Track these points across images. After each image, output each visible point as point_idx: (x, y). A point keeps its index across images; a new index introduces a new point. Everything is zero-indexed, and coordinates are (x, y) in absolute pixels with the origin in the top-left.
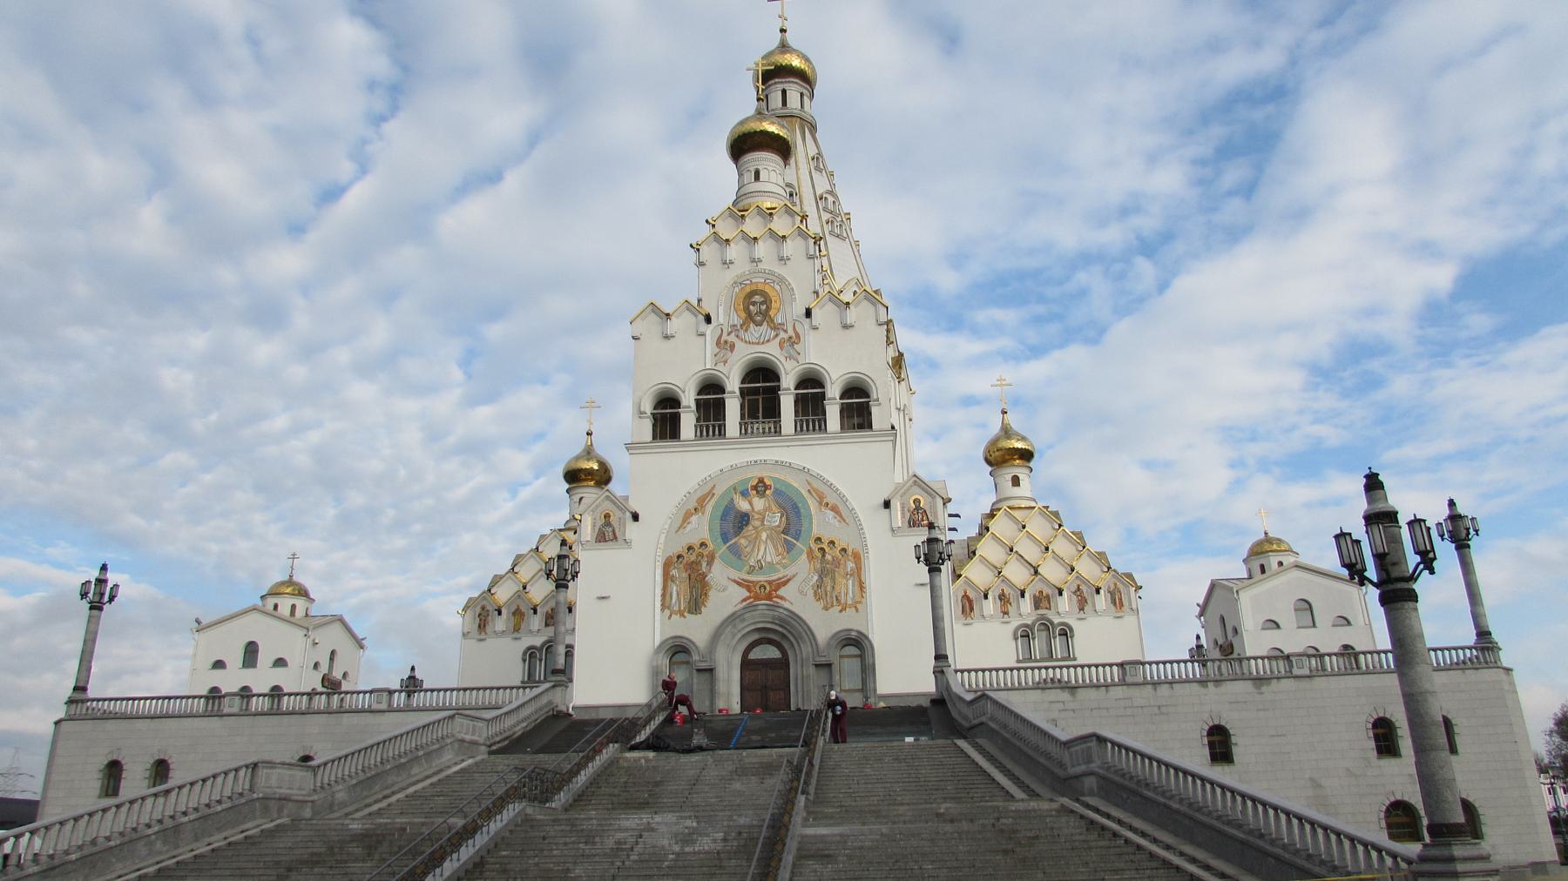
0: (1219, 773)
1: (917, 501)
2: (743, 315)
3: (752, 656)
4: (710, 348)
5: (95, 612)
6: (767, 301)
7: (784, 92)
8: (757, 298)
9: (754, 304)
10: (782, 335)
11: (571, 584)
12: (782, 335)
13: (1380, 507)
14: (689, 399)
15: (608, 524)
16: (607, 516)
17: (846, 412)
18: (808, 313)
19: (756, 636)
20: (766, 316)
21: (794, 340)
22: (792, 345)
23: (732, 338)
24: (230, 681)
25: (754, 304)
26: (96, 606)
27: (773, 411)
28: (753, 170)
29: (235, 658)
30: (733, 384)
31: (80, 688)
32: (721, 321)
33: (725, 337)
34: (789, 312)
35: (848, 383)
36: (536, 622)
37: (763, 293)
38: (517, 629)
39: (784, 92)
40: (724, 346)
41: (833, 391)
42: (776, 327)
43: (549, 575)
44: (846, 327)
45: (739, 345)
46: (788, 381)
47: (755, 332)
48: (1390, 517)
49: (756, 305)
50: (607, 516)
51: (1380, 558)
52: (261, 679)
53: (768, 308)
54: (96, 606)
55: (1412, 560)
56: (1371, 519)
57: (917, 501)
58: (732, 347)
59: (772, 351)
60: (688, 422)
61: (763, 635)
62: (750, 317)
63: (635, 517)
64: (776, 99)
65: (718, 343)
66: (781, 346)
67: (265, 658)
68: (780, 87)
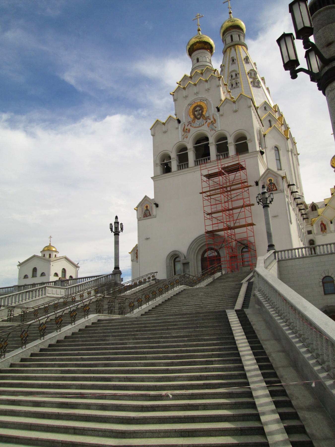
1: (270, 180)
2: (192, 117)
3: (206, 255)
5: (117, 236)
6: (202, 108)
7: (232, 37)
8: (198, 109)
11: (270, 205)
13: (94, 307)
14: (174, 155)
15: (147, 210)
16: (147, 207)
17: (207, 147)
18: (218, 110)
19: (206, 248)
20: (201, 115)
25: (196, 111)
26: (117, 234)
27: (207, 154)
28: (196, 58)
29: (30, 274)
30: (190, 146)
32: (184, 121)
34: (210, 111)
35: (236, 137)
39: (232, 37)
40: (186, 131)
41: (231, 140)
42: (207, 118)
46: (212, 140)
47: (197, 122)
48: (118, 223)
49: (198, 112)
50: (147, 207)
53: (202, 112)
54: (117, 234)
56: (115, 223)
57: (270, 180)
58: (189, 131)
59: (205, 130)
60: (174, 165)
61: (209, 247)
62: (195, 117)
63: (157, 205)
64: (228, 39)
65: (184, 130)
67: (39, 273)
68: (230, 34)
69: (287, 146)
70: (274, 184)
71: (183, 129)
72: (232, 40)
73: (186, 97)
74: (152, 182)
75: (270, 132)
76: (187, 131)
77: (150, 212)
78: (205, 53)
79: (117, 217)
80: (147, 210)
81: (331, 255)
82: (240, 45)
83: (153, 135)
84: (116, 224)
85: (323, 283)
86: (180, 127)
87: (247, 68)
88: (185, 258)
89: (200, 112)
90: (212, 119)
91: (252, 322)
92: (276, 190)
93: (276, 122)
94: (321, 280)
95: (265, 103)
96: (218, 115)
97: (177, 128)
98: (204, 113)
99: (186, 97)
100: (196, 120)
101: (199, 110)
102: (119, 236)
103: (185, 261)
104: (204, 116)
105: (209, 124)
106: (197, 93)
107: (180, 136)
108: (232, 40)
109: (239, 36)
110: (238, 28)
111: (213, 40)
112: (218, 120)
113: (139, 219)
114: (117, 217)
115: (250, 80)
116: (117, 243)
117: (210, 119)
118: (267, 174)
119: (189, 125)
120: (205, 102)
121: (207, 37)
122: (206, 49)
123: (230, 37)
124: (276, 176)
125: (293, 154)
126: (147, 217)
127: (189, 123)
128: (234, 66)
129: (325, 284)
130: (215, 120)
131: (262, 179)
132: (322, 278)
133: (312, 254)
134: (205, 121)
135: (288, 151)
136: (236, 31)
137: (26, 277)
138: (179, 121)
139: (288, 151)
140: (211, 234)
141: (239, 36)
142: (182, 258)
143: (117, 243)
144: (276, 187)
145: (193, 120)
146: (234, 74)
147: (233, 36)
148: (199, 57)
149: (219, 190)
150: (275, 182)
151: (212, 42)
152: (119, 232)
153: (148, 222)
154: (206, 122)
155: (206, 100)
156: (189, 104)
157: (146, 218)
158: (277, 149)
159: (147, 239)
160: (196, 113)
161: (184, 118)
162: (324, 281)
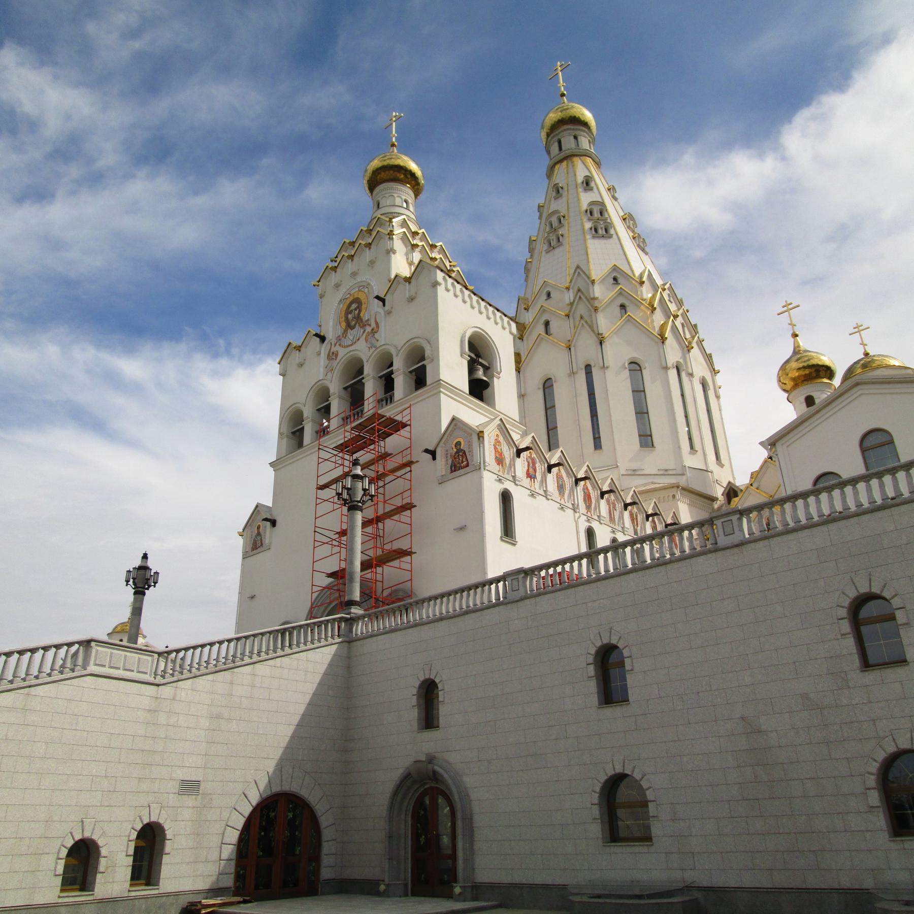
0: (574, 133)
2: (344, 324)
7: (560, 142)
8: (354, 306)
15: (259, 534)
20: (358, 318)
25: (351, 312)
47: (351, 334)
59: (362, 350)
64: (555, 148)
68: (556, 138)
69: (662, 356)
70: (464, 453)
72: (560, 149)
73: (337, 286)
74: (271, 472)
75: (617, 332)
78: (392, 188)
79: (145, 557)
80: (259, 534)
81: (440, 623)
82: (577, 156)
83: (283, 374)
87: (586, 199)
89: (357, 312)
90: (373, 325)
93: (639, 307)
95: (615, 268)
96: (382, 313)
98: (361, 315)
99: (337, 286)
100: (349, 331)
102: (146, 598)
104: (362, 320)
105: (369, 334)
106: (354, 275)
107: (322, 369)
108: (560, 149)
109: (576, 138)
110: (576, 122)
111: (417, 164)
113: (245, 556)
114: (145, 557)
115: (588, 225)
117: (370, 325)
118: (453, 431)
120: (366, 290)
121: (406, 158)
122: (402, 182)
123: (556, 144)
125: (683, 374)
127: (339, 339)
130: (377, 324)
131: (442, 444)
135: (666, 368)
136: (565, 130)
138: (323, 339)
139: (666, 368)
141: (576, 138)
144: (467, 460)
145: (345, 333)
151: (413, 166)
153: (262, 557)
157: (255, 552)
158: (635, 367)
161: (331, 329)
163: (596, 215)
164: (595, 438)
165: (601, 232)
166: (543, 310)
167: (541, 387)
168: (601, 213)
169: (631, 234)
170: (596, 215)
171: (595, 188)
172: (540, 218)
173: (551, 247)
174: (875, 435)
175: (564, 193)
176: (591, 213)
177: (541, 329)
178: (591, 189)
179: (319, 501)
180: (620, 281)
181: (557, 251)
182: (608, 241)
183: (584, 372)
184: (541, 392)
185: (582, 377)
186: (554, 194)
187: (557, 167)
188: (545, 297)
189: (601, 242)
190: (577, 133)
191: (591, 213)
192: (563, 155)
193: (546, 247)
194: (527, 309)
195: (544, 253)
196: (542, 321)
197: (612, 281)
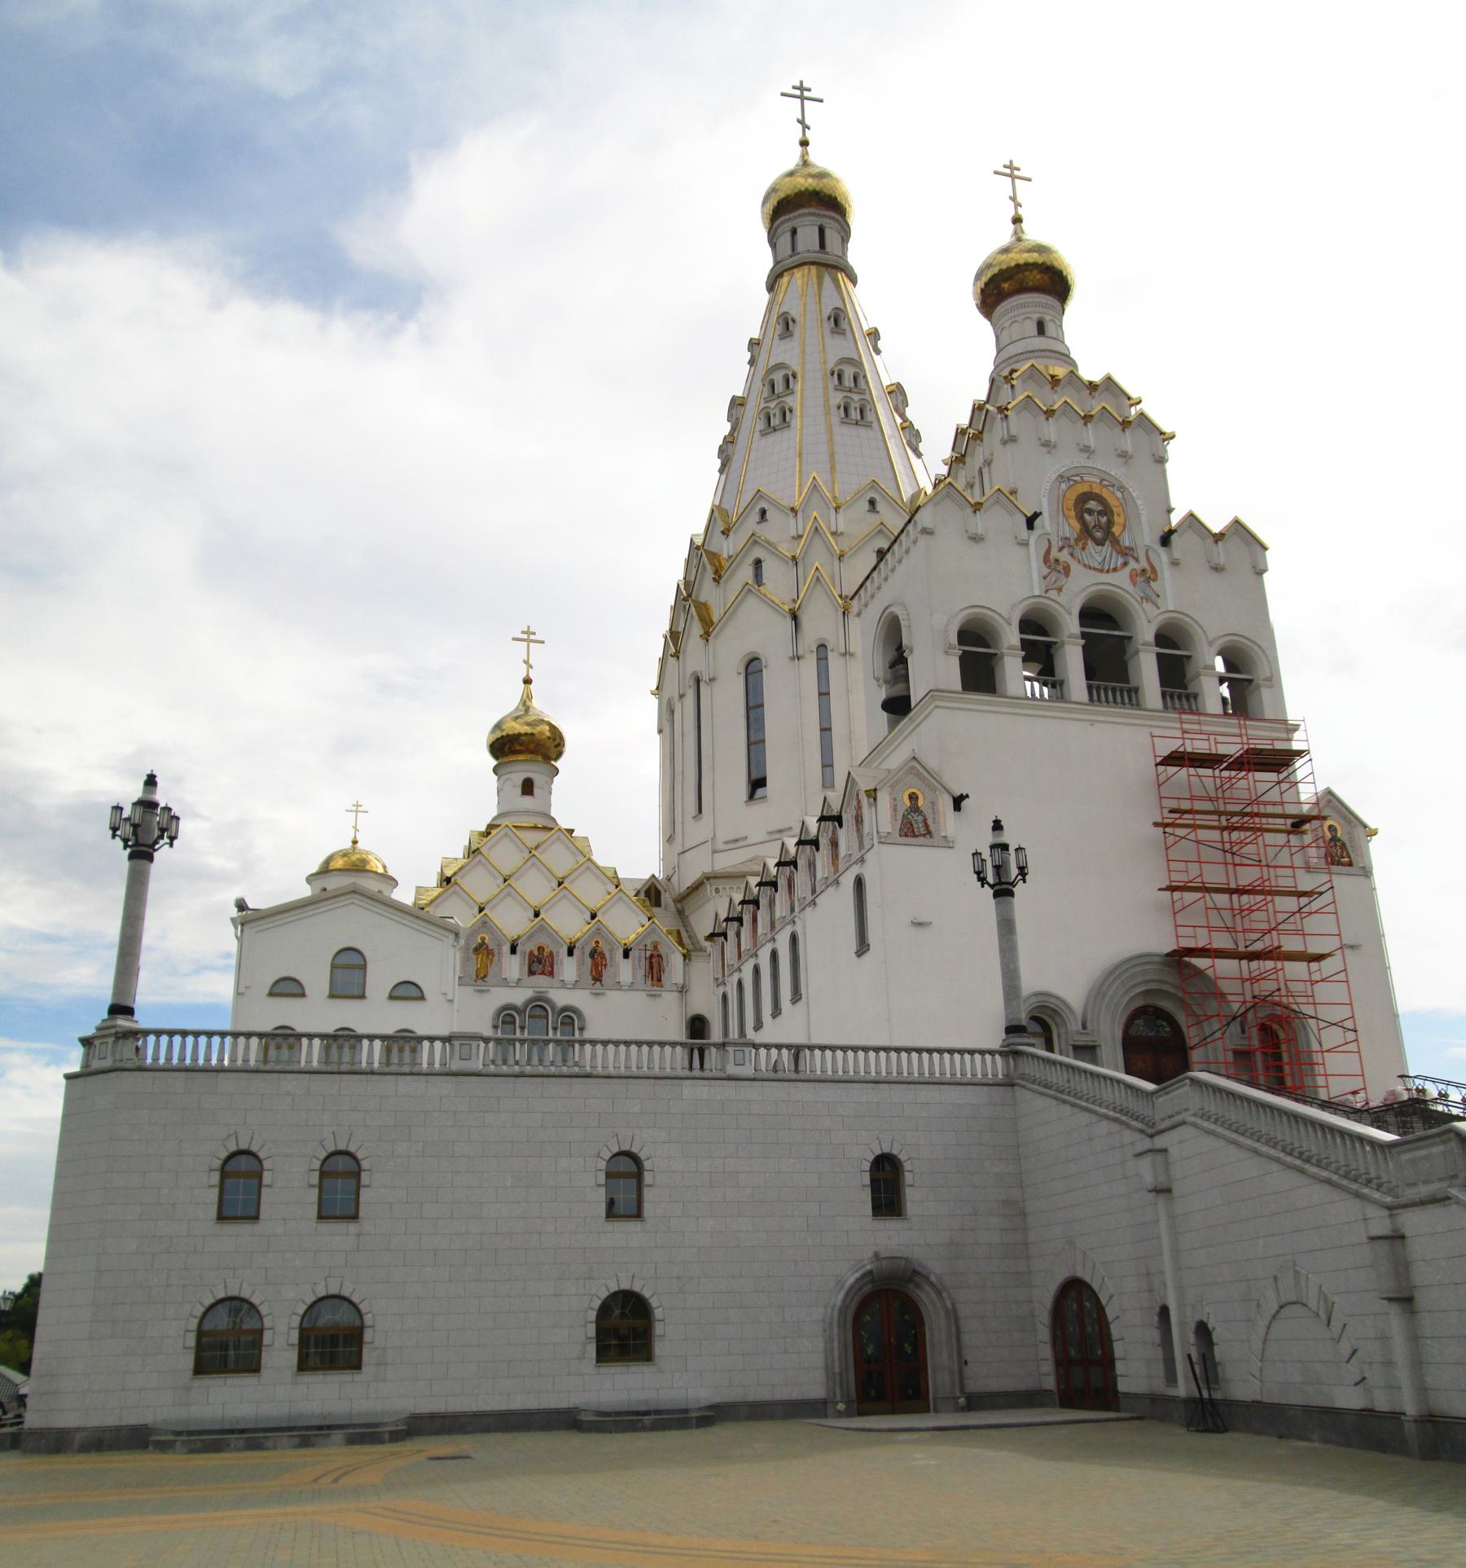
0: (820, 221)
2: (1077, 526)
3: (207, 1326)
4: (1036, 567)
7: (794, 232)
8: (1092, 504)
9: (1090, 512)
10: (1132, 564)
12: (1132, 564)
15: (915, 809)
16: (913, 797)
21: (1149, 575)
22: (1148, 580)
23: (1064, 556)
24: (317, 1014)
25: (1090, 512)
26: (1003, 891)
29: (317, 980)
31: (120, 1009)
32: (1049, 529)
33: (1054, 553)
36: (513, 967)
37: (1099, 499)
38: (481, 976)
42: (1127, 553)
43: (982, 880)
44: (1217, 569)
45: (1075, 568)
46: (1145, 631)
47: (1096, 554)
50: (913, 797)
51: (998, 869)
52: (375, 1016)
53: (1110, 523)
55: (1014, 871)
58: (1067, 571)
59: (1120, 583)
62: (1086, 531)
65: (1046, 559)
66: (1133, 576)
67: (379, 981)
68: (788, 226)
70: (1344, 844)
71: (1042, 553)
76: (1060, 568)
77: (930, 822)
80: (915, 809)
84: (997, 852)
85: (224, 1174)
86: (1032, 542)
88: (1084, 1027)
89: (1104, 520)
91: (840, 1283)
92: (1350, 864)
94: (317, 1164)
97: (1025, 544)
99: (1086, 450)
101: (1100, 513)
103: (1083, 1040)
104: (1118, 542)
107: (1036, 576)
112: (1166, 573)
116: (1007, 927)
117: (1137, 560)
119: (1066, 551)
120: (1119, 495)
123: (788, 235)
124: (1350, 823)
126: (915, 836)
127: (1066, 544)
128: (788, 344)
129: (326, 1182)
132: (224, 1155)
133: (691, 1068)
134: (1120, 561)
137: (288, 988)
140: (1178, 959)
142: (1074, 1026)
143: (1007, 927)
146: (778, 377)
147: (817, 248)
148: (1047, 318)
149: (1281, 821)
150: (1345, 839)
152: (1013, 884)
154: (1125, 564)
155: (1122, 488)
156: (1061, 476)
159: (920, 924)
160: (1086, 516)
162: (227, 1168)
163: (848, 381)
164: (748, 709)
165: (855, 415)
166: (754, 540)
167: (742, 670)
168: (855, 379)
169: (899, 420)
170: (848, 381)
171: (848, 332)
172: (752, 362)
173: (769, 428)
174: (341, 1158)
175: (796, 330)
176: (840, 377)
177: (746, 573)
178: (869, 426)
179: (1342, 977)
180: (879, 507)
181: (778, 435)
182: (862, 431)
183: (814, 657)
184: (742, 678)
185: (810, 666)
186: (780, 329)
187: (785, 279)
188: (757, 518)
189: (852, 430)
190: (826, 222)
191: (840, 377)
192: (796, 259)
193: (761, 425)
194: (726, 533)
195: (757, 434)
196: (750, 559)
197: (866, 506)
